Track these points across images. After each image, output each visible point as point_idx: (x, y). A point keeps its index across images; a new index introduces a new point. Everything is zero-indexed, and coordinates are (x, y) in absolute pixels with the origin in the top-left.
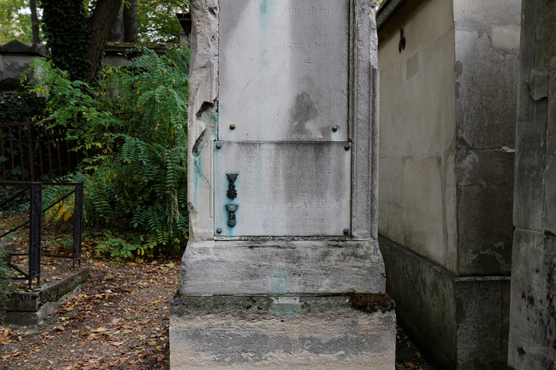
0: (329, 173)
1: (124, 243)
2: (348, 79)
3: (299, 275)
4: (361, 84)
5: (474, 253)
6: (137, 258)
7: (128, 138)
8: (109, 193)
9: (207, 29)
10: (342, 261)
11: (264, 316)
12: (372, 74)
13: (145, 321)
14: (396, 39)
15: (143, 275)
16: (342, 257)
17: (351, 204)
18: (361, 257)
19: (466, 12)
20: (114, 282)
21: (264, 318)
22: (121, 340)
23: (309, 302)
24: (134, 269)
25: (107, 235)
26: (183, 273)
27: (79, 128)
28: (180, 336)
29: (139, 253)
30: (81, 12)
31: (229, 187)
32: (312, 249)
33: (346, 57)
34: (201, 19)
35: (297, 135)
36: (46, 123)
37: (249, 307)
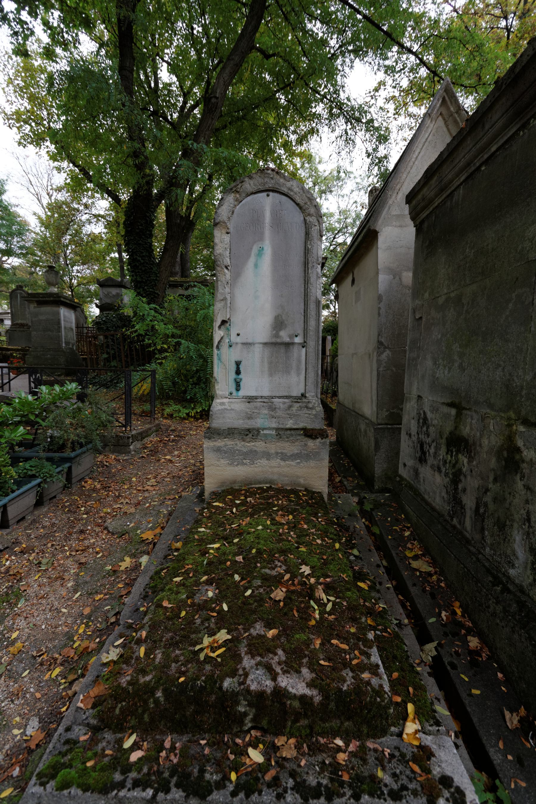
1: (181, 409)
5: (387, 411)
7: (183, 341)
13: (194, 453)
14: (350, 279)
27: (152, 335)
36: (131, 333)
37: (247, 435)
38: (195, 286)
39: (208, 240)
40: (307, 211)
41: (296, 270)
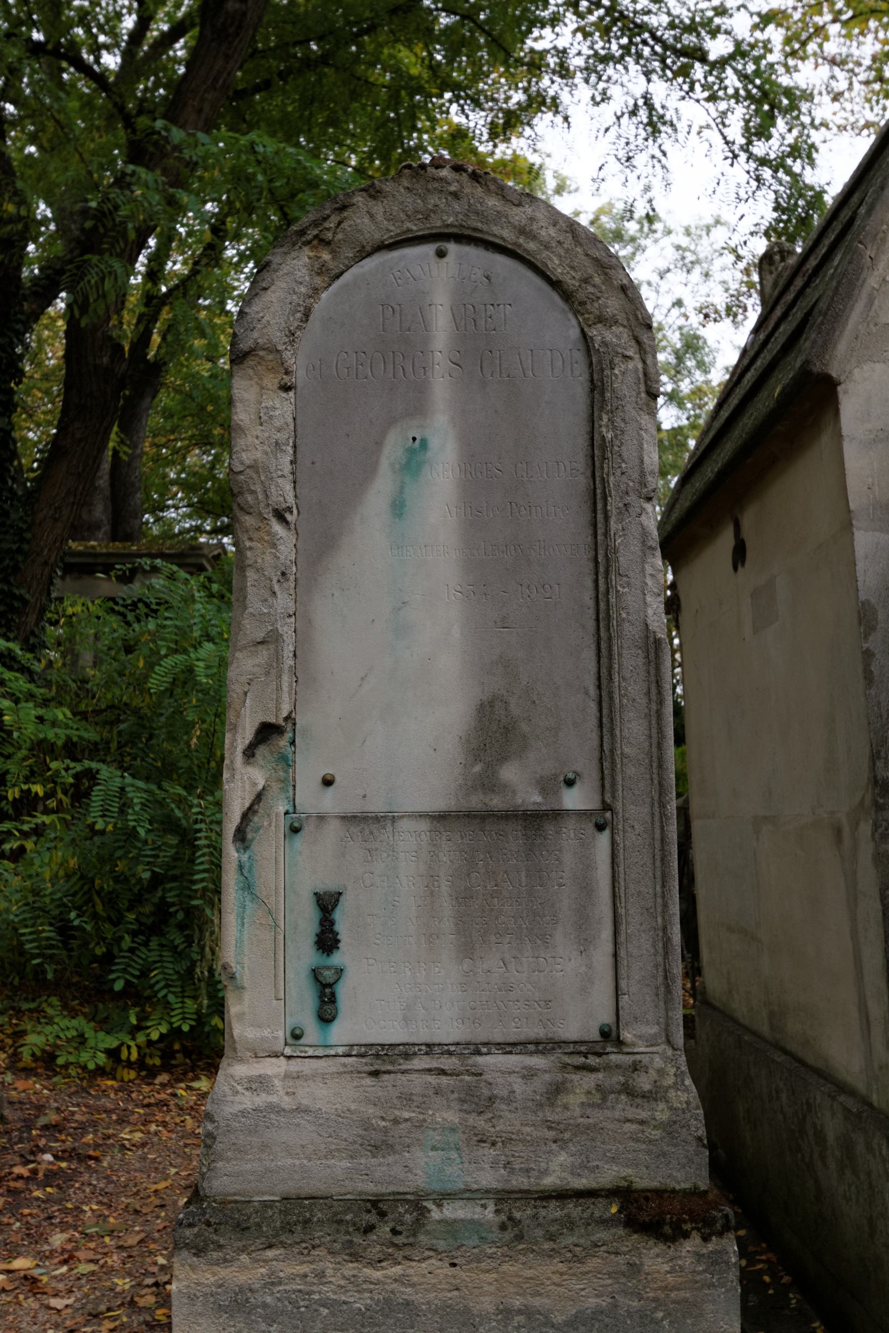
0: (560, 885)
2: (599, 662)
3: (494, 1144)
4: (628, 675)
6: (120, 1069)
7: (105, 771)
8: (59, 906)
9: (268, 558)
10: (599, 1106)
11: (407, 1252)
12: (652, 651)
13: (132, 1240)
14: (725, 541)
15: (133, 1113)
16: (598, 1096)
17: (616, 961)
18: (643, 1097)
19: (876, 489)
20: (60, 1132)
21: (406, 1258)
22: (70, 1291)
23: (517, 1215)
24: (112, 1095)
25: (49, 1011)
26: (209, 1142)
28: (199, 1308)
29: (124, 1055)
30: (10, 482)
31: (321, 923)
32: (524, 1077)
33: (591, 612)
34: (255, 535)
35: (481, 797)
37: (369, 1229)
38: (155, 570)
39: (211, 420)
40: (593, 308)
41: (560, 519)
